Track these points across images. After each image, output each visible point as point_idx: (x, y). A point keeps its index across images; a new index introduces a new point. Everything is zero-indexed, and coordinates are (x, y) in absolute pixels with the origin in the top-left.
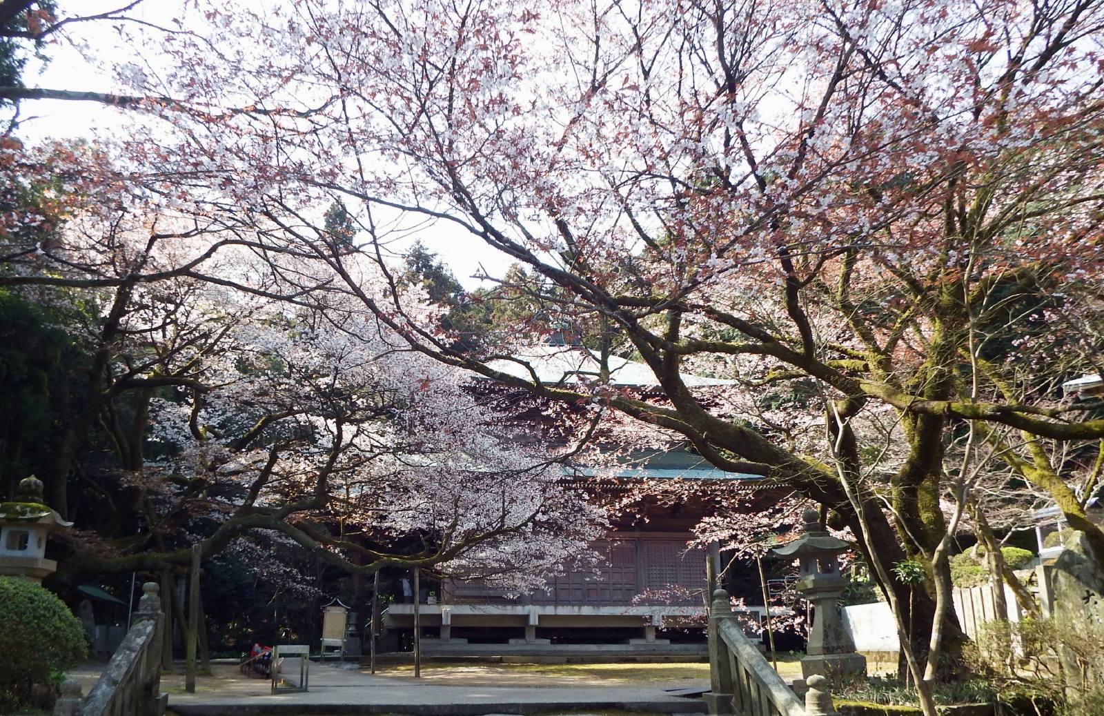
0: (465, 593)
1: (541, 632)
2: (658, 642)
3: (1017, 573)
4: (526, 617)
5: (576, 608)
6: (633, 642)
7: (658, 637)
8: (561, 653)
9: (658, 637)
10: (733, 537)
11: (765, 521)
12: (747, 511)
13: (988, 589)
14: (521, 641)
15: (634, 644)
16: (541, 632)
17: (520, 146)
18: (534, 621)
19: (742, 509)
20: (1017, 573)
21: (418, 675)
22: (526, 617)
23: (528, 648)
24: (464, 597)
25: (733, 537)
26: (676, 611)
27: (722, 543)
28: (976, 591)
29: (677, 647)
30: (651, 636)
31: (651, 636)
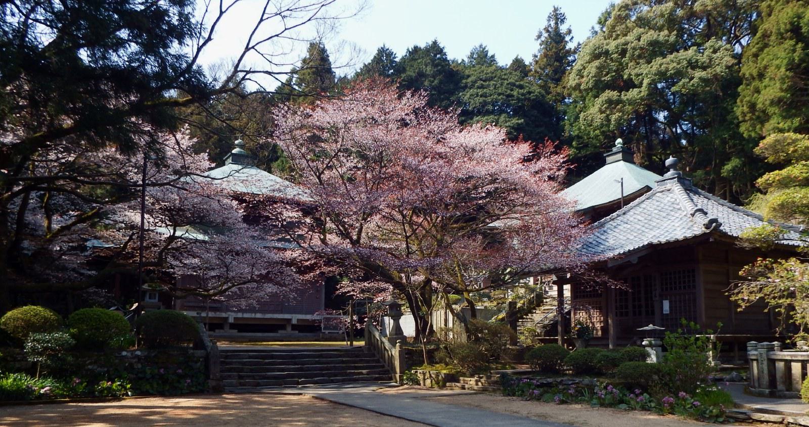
0: (191, 304)
1: (233, 326)
2: (293, 332)
3: (454, 306)
4: (227, 319)
5: (253, 315)
6: (280, 332)
7: (293, 329)
8: (243, 337)
9: (293, 329)
10: (353, 290)
11: (367, 285)
12: (361, 281)
13: (443, 312)
14: (221, 331)
15: (281, 333)
16: (233, 326)
17: (625, 398)
18: (231, 320)
19: (358, 280)
20: (454, 306)
21: (451, 330)
22: (227, 319)
23: (225, 334)
24: (189, 307)
25: (353, 290)
26: (240, 315)
27: (349, 292)
28: (439, 312)
29: (301, 334)
30: (289, 329)
31: (289, 329)
